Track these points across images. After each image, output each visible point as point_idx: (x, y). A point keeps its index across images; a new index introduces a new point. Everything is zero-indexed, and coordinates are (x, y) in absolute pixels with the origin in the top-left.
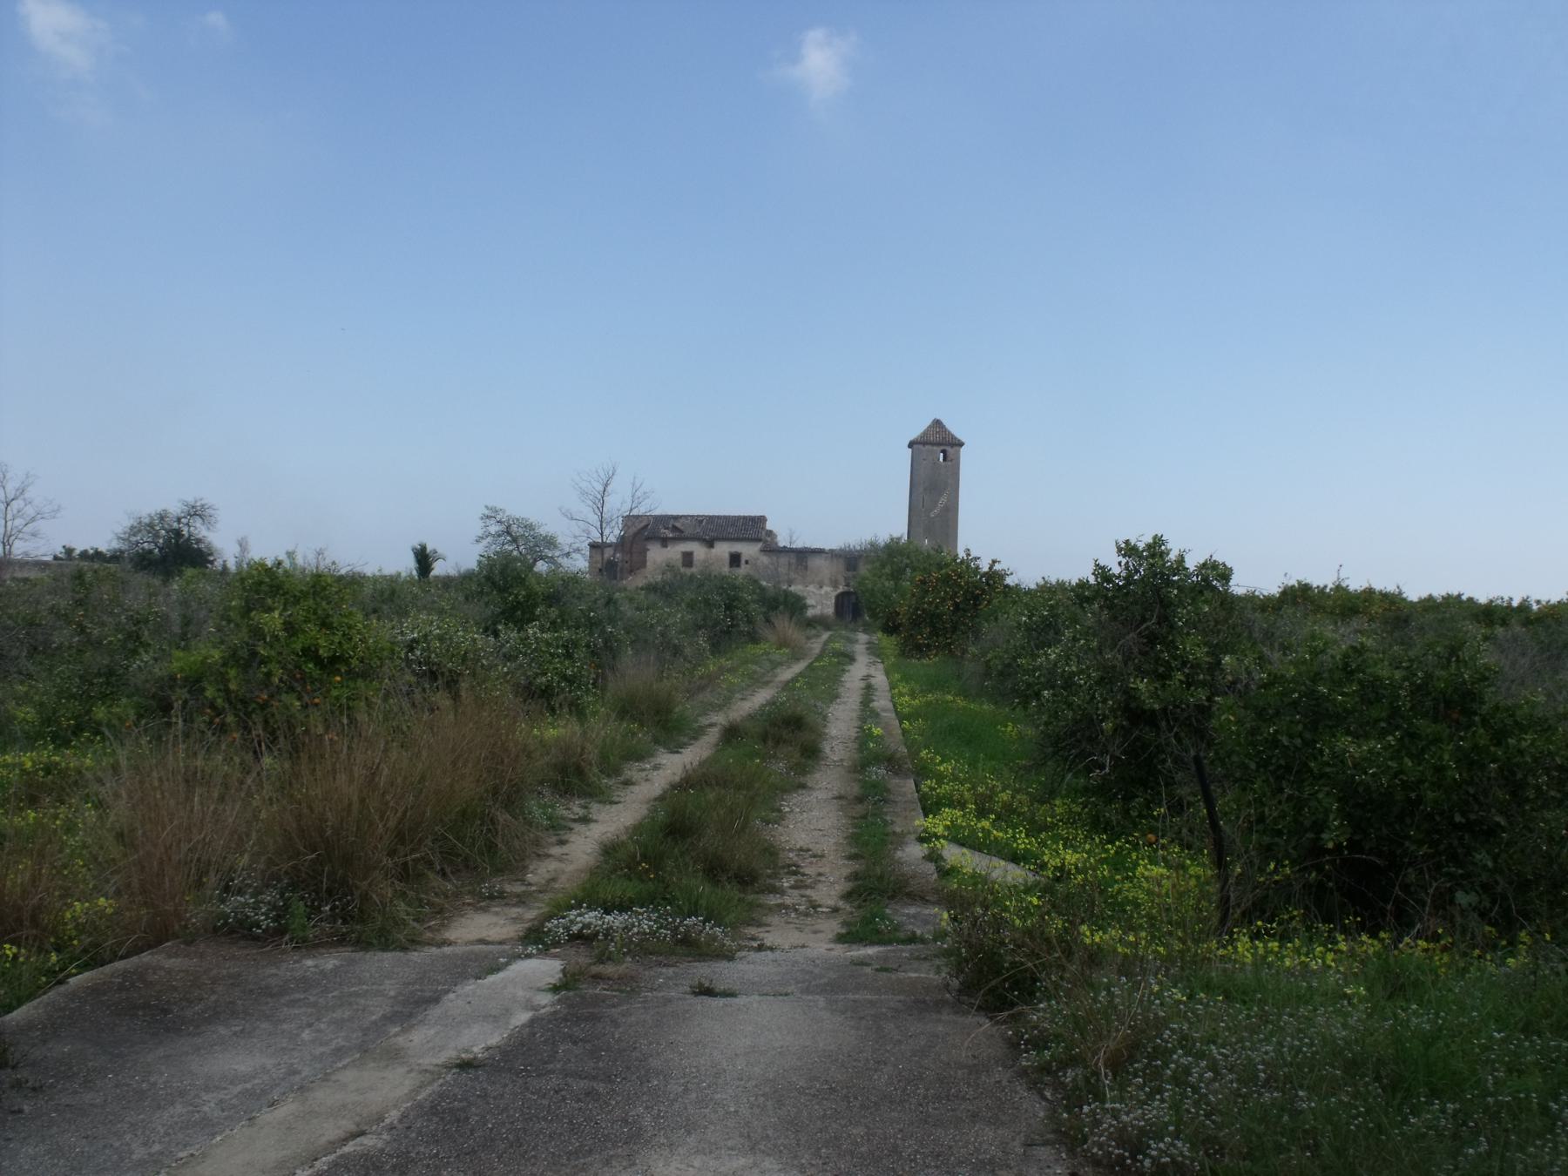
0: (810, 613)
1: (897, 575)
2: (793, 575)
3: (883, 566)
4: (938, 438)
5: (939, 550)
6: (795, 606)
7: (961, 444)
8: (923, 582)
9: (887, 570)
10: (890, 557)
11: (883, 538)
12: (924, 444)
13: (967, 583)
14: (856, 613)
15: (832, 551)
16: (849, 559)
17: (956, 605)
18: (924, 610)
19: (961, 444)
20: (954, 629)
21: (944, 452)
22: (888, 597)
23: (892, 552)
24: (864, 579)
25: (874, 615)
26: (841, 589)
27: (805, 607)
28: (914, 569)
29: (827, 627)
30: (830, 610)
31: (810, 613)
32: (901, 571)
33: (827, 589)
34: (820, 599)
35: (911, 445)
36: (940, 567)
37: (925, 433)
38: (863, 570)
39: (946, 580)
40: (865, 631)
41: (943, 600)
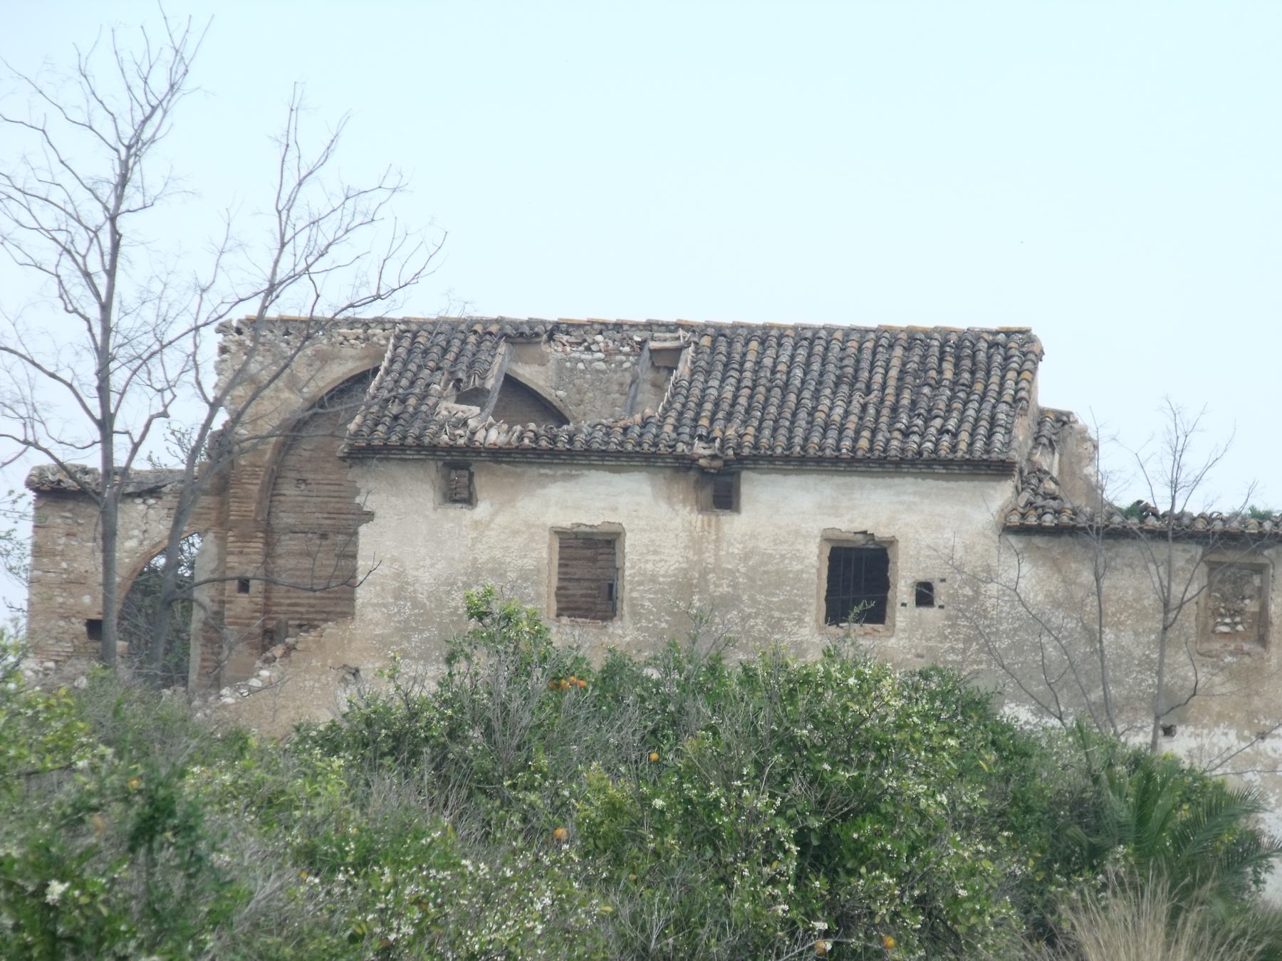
2: (1184, 670)
27: (1250, 853)
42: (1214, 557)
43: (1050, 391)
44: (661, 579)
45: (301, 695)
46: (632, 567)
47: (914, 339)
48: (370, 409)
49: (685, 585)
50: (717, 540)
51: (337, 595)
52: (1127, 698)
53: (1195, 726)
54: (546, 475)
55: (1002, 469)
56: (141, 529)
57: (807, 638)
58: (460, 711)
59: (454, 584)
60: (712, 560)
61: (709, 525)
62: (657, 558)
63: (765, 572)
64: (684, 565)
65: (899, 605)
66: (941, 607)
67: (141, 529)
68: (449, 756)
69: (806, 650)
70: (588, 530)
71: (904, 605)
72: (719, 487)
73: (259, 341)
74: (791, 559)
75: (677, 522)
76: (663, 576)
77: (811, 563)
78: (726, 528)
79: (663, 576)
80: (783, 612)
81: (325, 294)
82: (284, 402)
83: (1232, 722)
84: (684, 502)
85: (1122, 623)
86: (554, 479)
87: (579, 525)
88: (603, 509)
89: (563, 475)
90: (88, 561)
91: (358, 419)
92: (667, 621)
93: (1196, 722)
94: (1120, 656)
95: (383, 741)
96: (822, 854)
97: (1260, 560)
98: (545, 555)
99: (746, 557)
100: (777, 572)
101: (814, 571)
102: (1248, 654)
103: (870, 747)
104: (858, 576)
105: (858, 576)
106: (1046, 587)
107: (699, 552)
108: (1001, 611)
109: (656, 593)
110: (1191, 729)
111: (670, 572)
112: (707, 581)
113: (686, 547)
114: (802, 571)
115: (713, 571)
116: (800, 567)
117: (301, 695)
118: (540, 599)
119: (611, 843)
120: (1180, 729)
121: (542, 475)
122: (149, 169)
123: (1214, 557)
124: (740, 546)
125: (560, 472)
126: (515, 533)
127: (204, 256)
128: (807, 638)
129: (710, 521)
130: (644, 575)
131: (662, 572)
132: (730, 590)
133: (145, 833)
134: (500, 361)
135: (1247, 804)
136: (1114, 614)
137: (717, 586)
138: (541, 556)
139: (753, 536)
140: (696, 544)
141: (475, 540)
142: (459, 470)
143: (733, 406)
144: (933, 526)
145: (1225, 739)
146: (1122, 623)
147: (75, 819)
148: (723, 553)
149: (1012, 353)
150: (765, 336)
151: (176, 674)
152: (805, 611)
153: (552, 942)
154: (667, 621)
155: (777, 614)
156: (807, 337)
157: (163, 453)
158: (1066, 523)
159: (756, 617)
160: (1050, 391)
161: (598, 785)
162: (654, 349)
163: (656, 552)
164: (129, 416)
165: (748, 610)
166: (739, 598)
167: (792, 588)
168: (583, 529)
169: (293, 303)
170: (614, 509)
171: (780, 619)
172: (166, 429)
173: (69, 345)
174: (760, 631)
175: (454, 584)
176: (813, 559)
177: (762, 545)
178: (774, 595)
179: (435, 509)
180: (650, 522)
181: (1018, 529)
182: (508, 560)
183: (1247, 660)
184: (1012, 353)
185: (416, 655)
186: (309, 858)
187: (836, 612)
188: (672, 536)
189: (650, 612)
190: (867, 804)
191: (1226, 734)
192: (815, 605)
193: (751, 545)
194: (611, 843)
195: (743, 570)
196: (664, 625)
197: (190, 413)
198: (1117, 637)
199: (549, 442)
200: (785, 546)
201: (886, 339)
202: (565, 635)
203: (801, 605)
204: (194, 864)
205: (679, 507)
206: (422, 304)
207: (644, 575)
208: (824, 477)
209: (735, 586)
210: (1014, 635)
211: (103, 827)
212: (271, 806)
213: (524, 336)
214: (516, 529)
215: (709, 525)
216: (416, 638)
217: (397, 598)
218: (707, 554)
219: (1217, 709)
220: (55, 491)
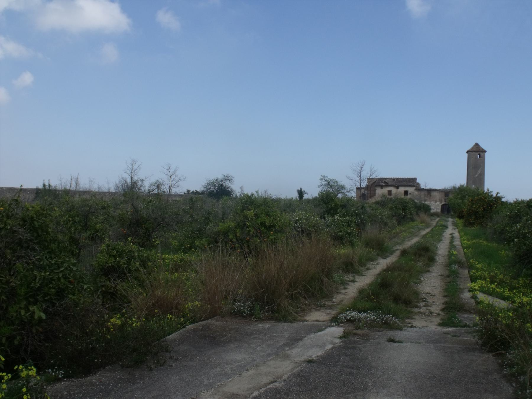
0: (432, 211)
1: (463, 198)
2: (426, 198)
3: (458, 195)
4: (477, 149)
5: (478, 189)
6: (426, 209)
7: (485, 152)
8: (472, 200)
9: (459, 196)
10: (460, 191)
11: (458, 185)
12: (472, 152)
13: (488, 201)
14: (448, 211)
15: (440, 190)
16: (446, 193)
17: (484, 209)
18: (472, 210)
19: (485, 152)
20: (483, 217)
21: (479, 154)
22: (460, 206)
23: (461, 189)
24: (451, 199)
25: (455, 212)
26: (443, 203)
27: (430, 209)
28: (469, 196)
29: (438, 216)
30: (439, 210)
31: (432, 211)
32: (465, 197)
33: (438, 203)
34: (436, 206)
35: (467, 152)
36: (478, 195)
37: (472, 148)
38: (451, 196)
39: (480, 199)
40: (451, 218)
41: (479, 207)
43: (418, 181)
45: (372, 200)
47: (409, 178)
48: (376, 183)
49: (396, 193)
51: (374, 194)
55: (414, 186)
56: (363, 191)
57: (403, 196)
58: (382, 201)
67: (363, 191)
68: (382, 204)
72: (397, 187)
73: (370, 179)
77: (403, 192)
81: (373, 176)
82: (371, 183)
90: (359, 193)
91: (428, 230)
95: (377, 203)
96: (404, 209)
103: (406, 203)
104: (406, 193)
105: (406, 193)
117: (372, 200)
118: (387, 194)
119: (391, 209)
122: (363, 169)
127: (366, 174)
128: (403, 196)
133: (362, 208)
134: (384, 180)
135: (430, 206)
138: (387, 192)
142: (382, 187)
143: (398, 182)
144: (411, 190)
145: (429, 202)
147: (358, 207)
149: (415, 179)
150: (400, 178)
151: (365, 199)
156: (403, 178)
157: (364, 186)
158: (419, 189)
160: (418, 181)
161: (390, 205)
162: (394, 179)
164: (362, 184)
169: (372, 177)
172: (364, 185)
173: (358, 179)
180: (393, 190)
184: (415, 179)
186: (373, 210)
187: (405, 195)
190: (406, 206)
194: (391, 209)
197: (365, 184)
199: (387, 185)
201: (408, 178)
202: (388, 196)
204: (365, 210)
206: (379, 177)
211: (360, 208)
212: (370, 207)
213: (386, 179)
214: (385, 190)
220: (358, 189)
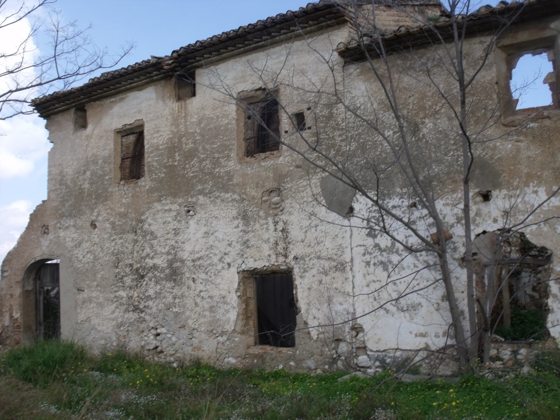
42: (507, 41)
44: (161, 147)
46: (148, 143)
50: (185, 116)
52: (448, 174)
53: (508, 189)
54: (112, 102)
59: (80, 172)
60: (183, 129)
61: (181, 108)
62: (158, 135)
63: (209, 130)
64: (171, 136)
65: (283, 133)
66: (310, 128)
69: (233, 176)
70: (130, 127)
71: (286, 132)
74: (222, 117)
75: (167, 112)
76: (162, 145)
78: (189, 107)
79: (162, 145)
80: (220, 153)
83: (540, 181)
84: (169, 98)
85: (437, 112)
86: (115, 102)
87: (125, 125)
88: (135, 113)
89: (120, 99)
92: (164, 172)
93: (509, 186)
94: (438, 139)
97: (547, 33)
98: (112, 146)
99: (200, 122)
100: (215, 128)
101: (234, 122)
102: (548, 117)
106: (379, 97)
107: (177, 126)
108: (349, 123)
109: (158, 156)
110: (504, 192)
111: (165, 142)
112: (181, 143)
113: (172, 124)
114: (228, 124)
115: (184, 135)
116: (227, 121)
120: (495, 193)
121: (111, 102)
123: (507, 41)
124: (196, 117)
125: (118, 98)
126: (101, 137)
129: (181, 105)
130: (153, 147)
131: (161, 143)
132: (192, 145)
136: (430, 107)
137: (186, 144)
139: (203, 108)
140: (175, 122)
141: (87, 146)
146: (437, 112)
148: (188, 123)
152: (231, 149)
153: (245, 405)
154: (164, 172)
155: (216, 155)
159: (206, 160)
163: (158, 132)
165: (202, 156)
166: (196, 150)
167: (224, 136)
168: (128, 127)
170: (140, 112)
171: (219, 158)
174: (208, 168)
175: (80, 172)
176: (234, 114)
177: (207, 113)
178: (214, 143)
179: (426, 344)
181: (351, 55)
182: (99, 153)
183: (547, 122)
185: (67, 214)
188: (165, 119)
189: (157, 168)
191: (536, 192)
192: (236, 146)
193: (201, 115)
195: (198, 131)
196: (163, 175)
198: (435, 124)
200: (219, 110)
203: (228, 146)
205: (167, 101)
207: (153, 147)
208: (237, 59)
209: (194, 143)
210: (359, 138)
215: (181, 108)
216: (67, 205)
217: (60, 185)
218: (181, 126)
219: (525, 171)
